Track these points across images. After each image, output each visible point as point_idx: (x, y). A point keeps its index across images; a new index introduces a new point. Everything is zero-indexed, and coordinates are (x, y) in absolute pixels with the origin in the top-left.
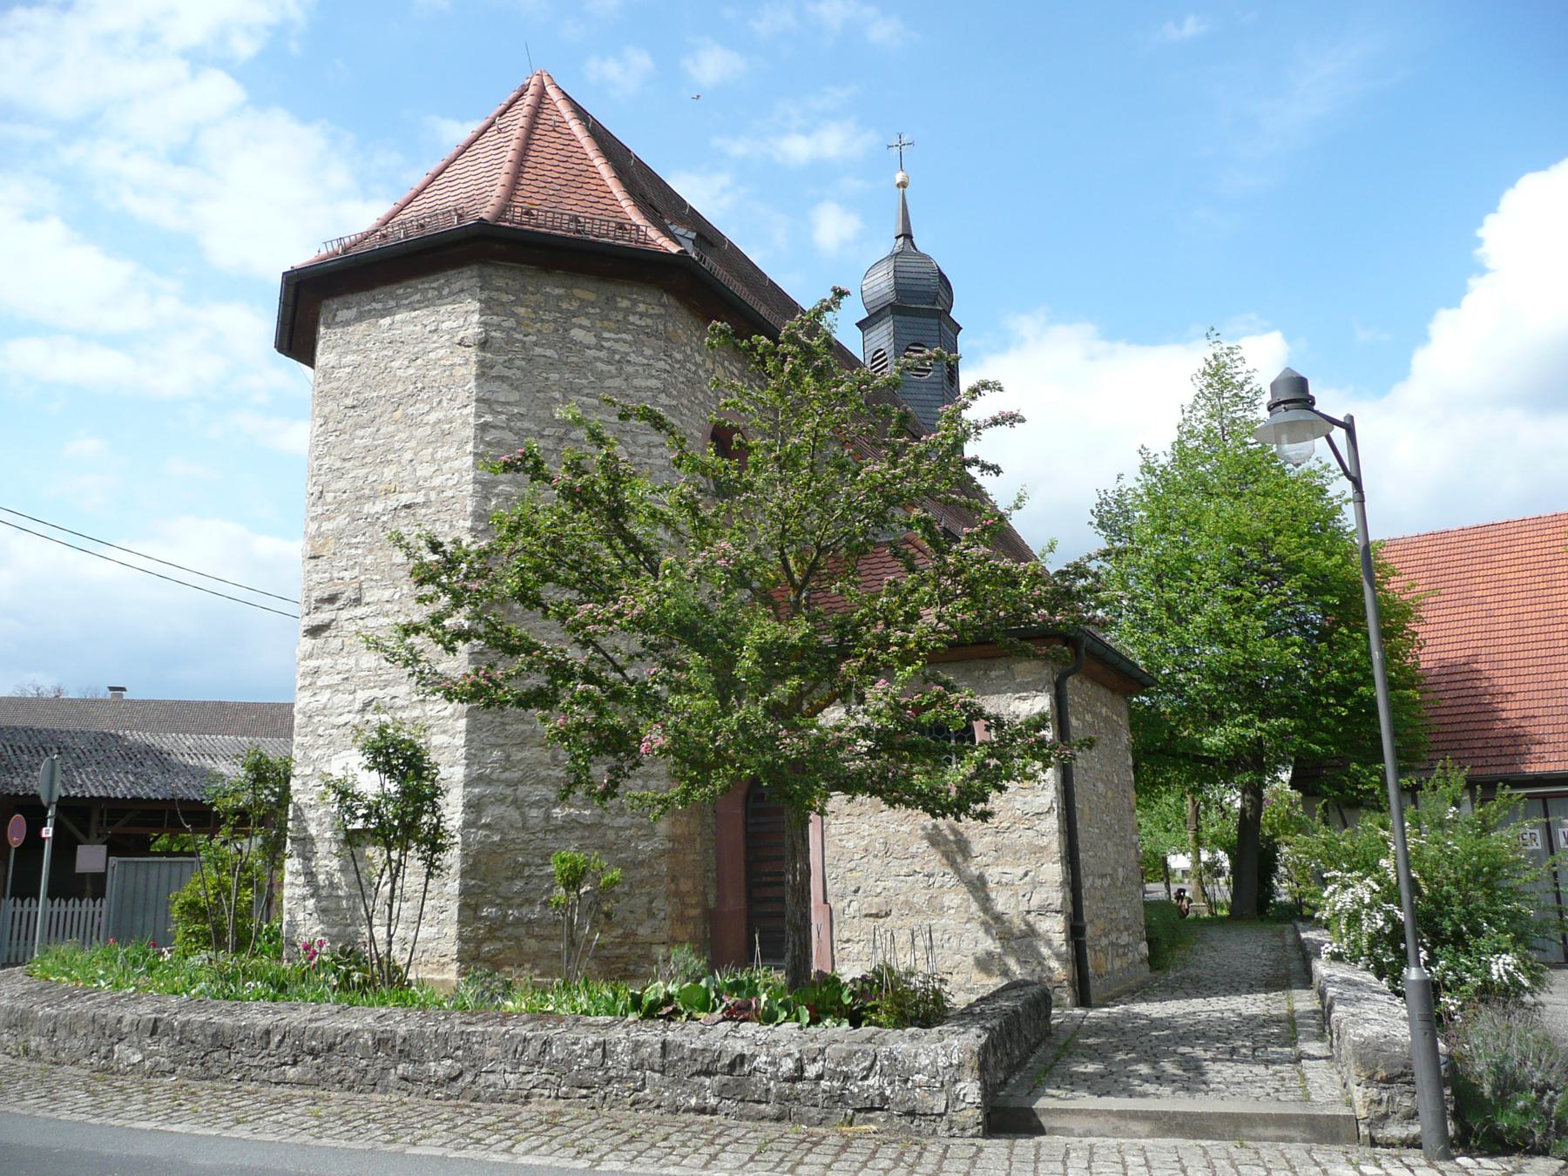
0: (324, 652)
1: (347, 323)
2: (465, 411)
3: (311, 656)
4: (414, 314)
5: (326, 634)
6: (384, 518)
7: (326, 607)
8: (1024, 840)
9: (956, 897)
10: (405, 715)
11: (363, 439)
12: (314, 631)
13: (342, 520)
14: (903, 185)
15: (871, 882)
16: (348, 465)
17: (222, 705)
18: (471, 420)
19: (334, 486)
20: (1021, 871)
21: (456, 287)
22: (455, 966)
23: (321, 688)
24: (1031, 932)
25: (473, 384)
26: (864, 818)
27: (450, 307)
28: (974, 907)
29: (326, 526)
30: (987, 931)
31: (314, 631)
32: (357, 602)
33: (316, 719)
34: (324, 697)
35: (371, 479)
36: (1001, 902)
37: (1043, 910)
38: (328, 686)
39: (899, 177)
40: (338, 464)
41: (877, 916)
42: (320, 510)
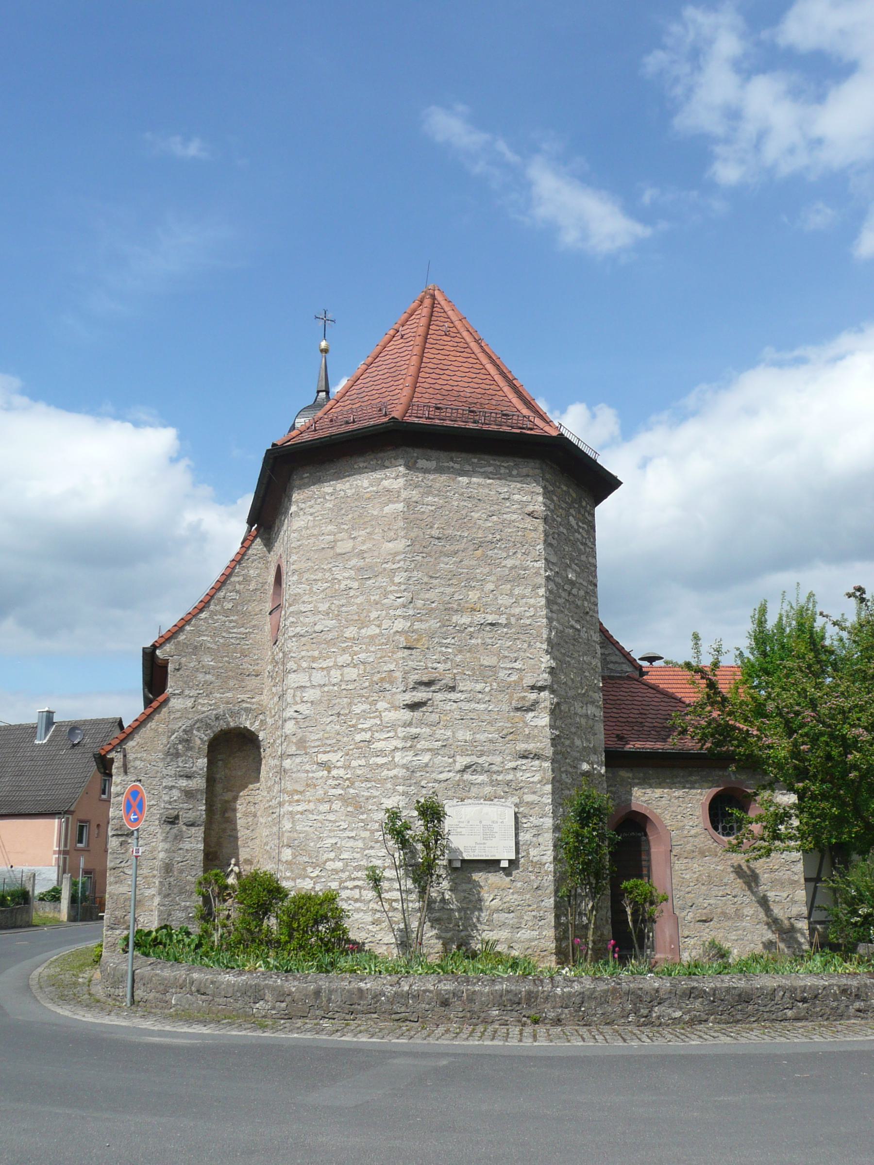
0: (421, 723)
1: (426, 471)
2: (537, 565)
3: (410, 724)
5: (424, 709)
6: (472, 629)
7: (423, 688)
8: (786, 877)
9: (752, 910)
10: (500, 778)
11: (446, 565)
12: (414, 706)
13: (434, 624)
14: (325, 351)
15: (701, 900)
16: (435, 582)
18: (542, 572)
19: (422, 596)
20: (786, 895)
21: (524, 471)
22: (554, 958)
24: (792, 929)
25: (541, 546)
26: (695, 860)
27: (519, 485)
28: (762, 915)
29: (417, 625)
31: (414, 706)
32: (453, 689)
33: (418, 774)
34: (426, 758)
35: (456, 597)
36: (777, 911)
37: (798, 917)
39: (323, 344)
40: (426, 579)
41: (705, 921)
42: (411, 612)
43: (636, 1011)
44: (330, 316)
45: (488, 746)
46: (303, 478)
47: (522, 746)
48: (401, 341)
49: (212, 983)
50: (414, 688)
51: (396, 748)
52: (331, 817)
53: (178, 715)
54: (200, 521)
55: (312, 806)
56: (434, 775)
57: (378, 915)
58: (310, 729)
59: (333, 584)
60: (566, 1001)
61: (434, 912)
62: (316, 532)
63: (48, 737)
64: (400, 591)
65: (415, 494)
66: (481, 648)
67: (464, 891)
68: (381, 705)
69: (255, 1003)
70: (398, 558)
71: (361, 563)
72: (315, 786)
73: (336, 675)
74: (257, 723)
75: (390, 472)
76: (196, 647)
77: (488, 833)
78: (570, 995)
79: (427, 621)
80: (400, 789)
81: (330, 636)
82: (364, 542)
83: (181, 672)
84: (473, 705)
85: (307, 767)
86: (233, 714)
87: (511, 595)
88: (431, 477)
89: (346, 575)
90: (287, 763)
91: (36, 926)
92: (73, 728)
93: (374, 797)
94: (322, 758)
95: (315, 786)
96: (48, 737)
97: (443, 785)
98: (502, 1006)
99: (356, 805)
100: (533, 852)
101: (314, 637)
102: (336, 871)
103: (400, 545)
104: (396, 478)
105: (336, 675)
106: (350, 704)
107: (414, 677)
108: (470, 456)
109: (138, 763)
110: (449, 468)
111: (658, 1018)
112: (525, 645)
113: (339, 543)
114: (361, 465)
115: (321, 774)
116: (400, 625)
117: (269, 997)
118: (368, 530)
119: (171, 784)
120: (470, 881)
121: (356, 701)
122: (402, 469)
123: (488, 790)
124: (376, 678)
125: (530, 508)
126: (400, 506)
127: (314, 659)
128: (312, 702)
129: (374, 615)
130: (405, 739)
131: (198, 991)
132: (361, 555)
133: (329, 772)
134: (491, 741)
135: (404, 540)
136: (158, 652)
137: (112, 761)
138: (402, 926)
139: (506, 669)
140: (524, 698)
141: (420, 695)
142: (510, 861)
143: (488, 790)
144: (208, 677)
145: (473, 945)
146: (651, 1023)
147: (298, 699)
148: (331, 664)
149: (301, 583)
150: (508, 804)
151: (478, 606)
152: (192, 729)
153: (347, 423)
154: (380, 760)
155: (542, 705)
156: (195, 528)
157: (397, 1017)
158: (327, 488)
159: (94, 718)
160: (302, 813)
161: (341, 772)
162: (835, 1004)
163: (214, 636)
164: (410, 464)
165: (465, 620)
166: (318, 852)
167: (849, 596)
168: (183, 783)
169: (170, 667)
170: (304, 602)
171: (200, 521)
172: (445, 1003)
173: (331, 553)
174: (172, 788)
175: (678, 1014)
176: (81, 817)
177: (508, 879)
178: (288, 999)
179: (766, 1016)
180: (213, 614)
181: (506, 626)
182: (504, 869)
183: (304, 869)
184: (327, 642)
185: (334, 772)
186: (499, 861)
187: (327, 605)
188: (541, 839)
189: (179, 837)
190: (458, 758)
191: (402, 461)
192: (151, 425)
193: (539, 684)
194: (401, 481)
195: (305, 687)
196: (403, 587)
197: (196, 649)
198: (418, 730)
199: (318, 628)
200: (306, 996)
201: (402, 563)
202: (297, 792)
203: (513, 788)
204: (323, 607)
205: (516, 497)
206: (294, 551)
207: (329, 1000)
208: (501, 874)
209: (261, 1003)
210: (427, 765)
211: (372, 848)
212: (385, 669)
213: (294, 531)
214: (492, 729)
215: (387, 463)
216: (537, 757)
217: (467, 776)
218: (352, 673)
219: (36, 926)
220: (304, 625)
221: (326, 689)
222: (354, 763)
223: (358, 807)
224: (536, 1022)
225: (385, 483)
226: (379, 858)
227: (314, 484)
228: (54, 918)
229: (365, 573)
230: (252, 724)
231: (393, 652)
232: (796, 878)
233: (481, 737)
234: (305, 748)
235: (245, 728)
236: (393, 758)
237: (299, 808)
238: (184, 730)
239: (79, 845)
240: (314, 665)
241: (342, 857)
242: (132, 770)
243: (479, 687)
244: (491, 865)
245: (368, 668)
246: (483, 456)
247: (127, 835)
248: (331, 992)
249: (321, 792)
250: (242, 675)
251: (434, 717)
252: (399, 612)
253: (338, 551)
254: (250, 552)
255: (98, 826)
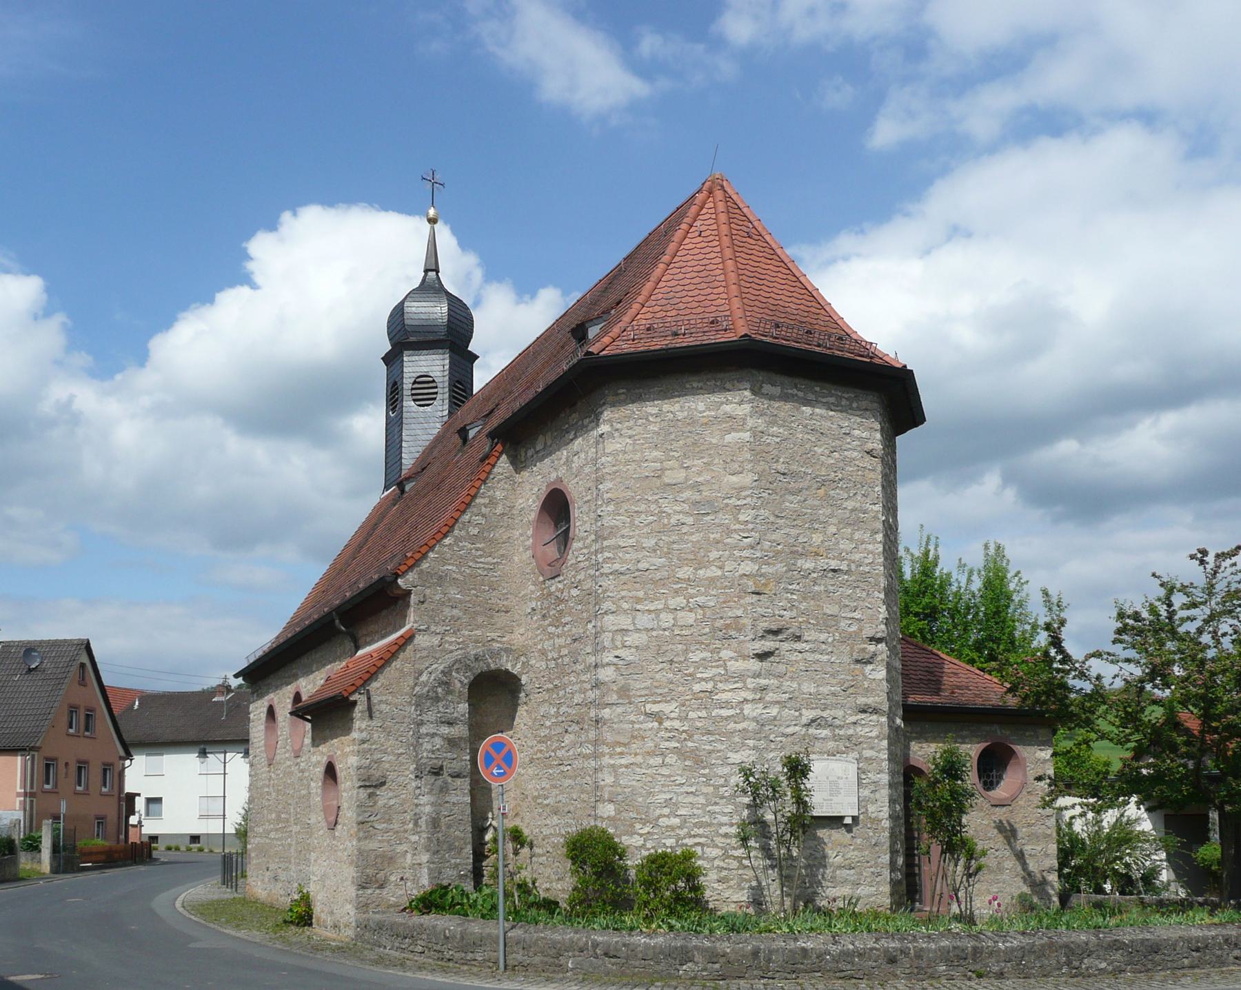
0: (770, 674)
1: (771, 398)
4: (831, 413)
5: (772, 659)
6: (815, 575)
7: (770, 637)
9: (1011, 863)
10: (841, 733)
11: (791, 503)
12: (763, 656)
13: (780, 568)
16: (781, 521)
17: (56, 641)
21: (864, 404)
23: (771, 703)
24: (1044, 882)
25: (879, 488)
27: (859, 420)
28: (1019, 868)
29: (765, 569)
30: (1025, 882)
32: (798, 638)
33: (767, 728)
34: (774, 711)
36: (1032, 866)
37: (1050, 870)
38: (778, 702)
39: (432, 212)
40: (772, 519)
42: (759, 555)
43: (1069, 963)
44: (438, 177)
45: (831, 700)
46: (617, 395)
47: (862, 700)
48: (700, 239)
49: (624, 945)
50: (763, 636)
51: (746, 700)
52: (665, 771)
53: (425, 653)
55: (639, 759)
56: (782, 729)
57: (724, 873)
58: (635, 677)
60: (1009, 955)
61: (783, 867)
64: (748, 531)
65: (760, 423)
69: (682, 965)
70: (743, 494)
71: (697, 497)
72: (643, 738)
74: (519, 666)
76: (441, 577)
77: (834, 789)
78: (1013, 949)
79: (774, 565)
80: (751, 743)
81: (658, 576)
82: (699, 474)
83: (425, 605)
84: (818, 656)
85: (632, 718)
86: (495, 654)
87: (851, 540)
88: (777, 405)
89: (678, 508)
91: (23, 879)
93: (719, 751)
94: (651, 708)
95: (643, 738)
97: (789, 739)
98: (949, 962)
99: (697, 760)
100: (871, 808)
101: (637, 577)
102: (672, 828)
103: (747, 479)
105: (667, 619)
106: (686, 651)
107: (763, 625)
108: (813, 383)
110: (793, 396)
111: (1087, 969)
113: (667, 473)
114: (695, 385)
115: (650, 725)
116: (748, 567)
117: (698, 957)
118: (705, 460)
119: (432, 731)
122: (747, 393)
123: (831, 745)
125: (869, 446)
126: (746, 436)
127: (638, 600)
128: (637, 647)
129: (714, 555)
130: (754, 690)
131: (606, 954)
132: (696, 486)
133: (660, 723)
134: (834, 694)
135: (751, 475)
136: (400, 581)
137: (355, 703)
138: (754, 883)
140: (864, 650)
142: (854, 818)
143: (831, 745)
144: (455, 612)
145: (818, 902)
147: (619, 644)
148: (661, 607)
149: (619, 514)
150: (849, 759)
151: (821, 550)
152: (450, 671)
154: (725, 713)
155: (879, 658)
156: (66, 407)
157: (842, 974)
158: (651, 408)
159: (68, 637)
160: (626, 767)
161: (677, 724)
162: (1219, 953)
164: (756, 389)
165: (808, 564)
166: (648, 808)
167: (1192, 557)
168: (445, 730)
169: (413, 599)
170: (623, 537)
172: (892, 961)
173: (658, 482)
174: (433, 735)
175: (1103, 965)
176: (48, 755)
178: (722, 960)
180: (458, 540)
181: (846, 573)
182: (846, 825)
183: (632, 826)
184: (654, 582)
185: (667, 724)
186: (842, 818)
187: (653, 542)
188: (878, 795)
189: (444, 789)
191: (748, 385)
193: (879, 635)
194: (747, 408)
195: (627, 630)
196: (750, 526)
197: (441, 579)
199: (642, 566)
200: (743, 956)
201: (749, 499)
202: (619, 744)
203: (852, 743)
204: (650, 543)
205: (856, 432)
206: (608, 477)
207: (769, 960)
208: (843, 830)
209: (690, 964)
210: (775, 718)
211: (716, 804)
212: (730, 614)
214: (834, 681)
215: (728, 385)
216: (876, 711)
217: (812, 731)
218: (690, 618)
219: (23, 879)
220: (623, 562)
221: (654, 633)
222: (692, 715)
223: (699, 762)
224: (980, 976)
226: (725, 814)
227: (633, 402)
229: (703, 508)
230: (514, 666)
231: (740, 597)
232: (1049, 832)
233: (825, 690)
234: (629, 697)
235: (507, 672)
236: (742, 710)
237: (623, 761)
238: (442, 672)
239: (46, 786)
240: (638, 607)
241: (679, 813)
242: (377, 714)
243: (823, 637)
244: (835, 821)
245: (708, 613)
247: (375, 786)
249: (651, 744)
250: (492, 611)
251: (782, 668)
252: (745, 553)
253: (667, 480)
255: (67, 764)
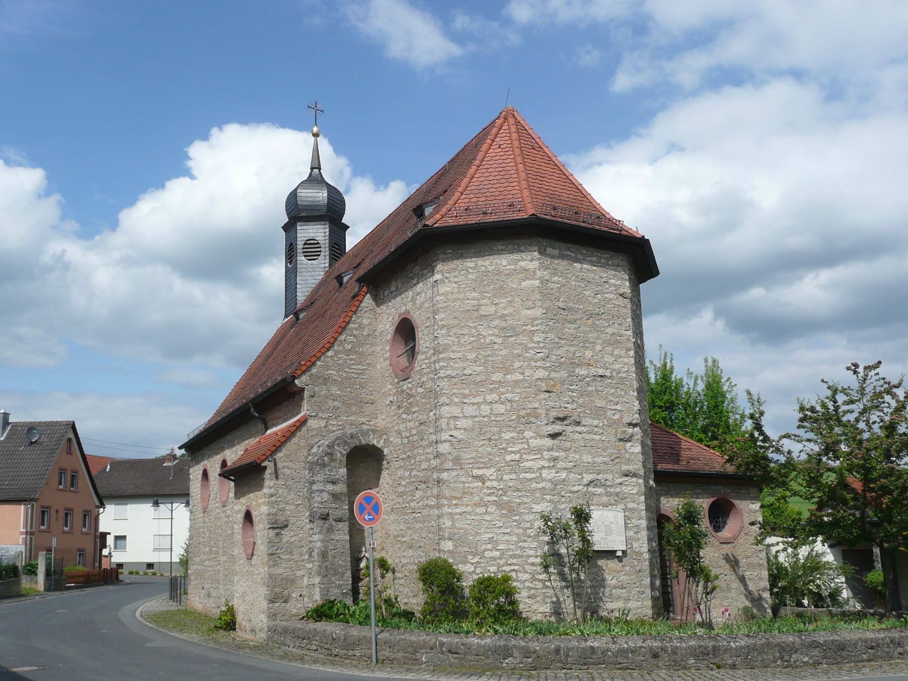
0: (559, 449)
3: (552, 449)
4: (595, 268)
5: (560, 438)
7: (559, 422)
10: (612, 490)
11: (570, 329)
12: (554, 436)
13: (564, 374)
16: (561, 341)
21: (617, 262)
24: (760, 598)
25: (629, 320)
27: (614, 273)
28: (742, 588)
29: (553, 375)
32: (578, 423)
33: (559, 487)
34: (563, 475)
36: (751, 587)
39: (315, 129)
40: (556, 340)
42: (548, 365)
43: (781, 658)
47: (625, 468)
48: (499, 150)
49: (463, 644)
51: (543, 467)
52: (487, 518)
53: (315, 432)
54: (64, 252)
55: (469, 509)
56: (569, 488)
57: (533, 591)
59: (479, 339)
62: (461, 296)
63: (5, 435)
64: (540, 348)
65: (546, 274)
66: (595, 394)
67: (593, 573)
68: (528, 434)
70: (536, 322)
71: (504, 324)
72: (472, 494)
73: (485, 410)
74: (382, 442)
75: (527, 256)
76: (325, 379)
77: (609, 531)
78: (741, 648)
80: (548, 497)
82: (505, 308)
83: (315, 398)
84: (593, 436)
85: (463, 479)
86: (365, 434)
87: (612, 355)
88: (556, 262)
90: (445, 475)
92: (31, 428)
93: (525, 503)
94: (479, 472)
95: (472, 494)
96: (5, 435)
97: (575, 495)
98: (696, 657)
99: (510, 510)
100: (635, 545)
101: (463, 379)
102: (494, 559)
103: (538, 312)
104: (531, 260)
105: (485, 410)
106: (500, 432)
107: (554, 414)
109: (286, 470)
110: (568, 256)
111: (795, 662)
112: (623, 393)
113: (482, 308)
114: (500, 248)
115: (476, 485)
116: (541, 374)
117: (516, 654)
119: (321, 488)
120: (597, 566)
121: (505, 430)
123: (605, 499)
124: (522, 413)
125: (622, 291)
126: (537, 283)
127: (465, 396)
128: (465, 429)
129: (517, 364)
130: (549, 460)
131: (449, 651)
132: (503, 317)
133: (483, 483)
134: (605, 463)
137: (265, 468)
138: (554, 599)
139: (611, 409)
140: (625, 432)
141: (557, 428)
142: (623, 551)
143: (605, 499)
144: (336, 403)
146: (791, 666)
147: (452, 426)
149: (450, 336)
151: (592, 362)
153: (485, 213)
155: (636, 438)
157: (620, 666)
158: (470, 263)
160: (460, 514)
161: (495, 484)
162: (887, 650)
163: (339, 371)
165: (583, 372)
167: (848, 369)
168: (330, 487)
170: (453, 351)
171: (64, 252)
172: (656, 656)
173: (476, 314)
174: (322, 491)
175: (806, 659)
176: (43, 504)
177: (620, 564)
178: (534, 656)
179: (853, 659)
180: (337, 353)
181: (610, 378)
182: (618, 557)
183: (465, 557)
184: (476, 383)
185: (488, 484)
187: (474, 355)
188: (639, 536)
189: (330, 530)
190: (584, 475)
191: (536, 248)
192: (20, 165)
193: (634, 422)
194: (536, 264)
196: (542, 345)
198: (557, 454)
199: (466, 372)
200: (548, 652)
203: (620, 498)
207: (567, 656)
208: (616, 561)
209: (510, 659)
210: (564, 480)
211: (525, 541)
213: (441, 295)
214: (605, 454)
216: (635, 475)
217: (591, 489)
218: (502, 409)
220: (454, 369)
221: (477, 419)
222: (506, 477)
223: (512, 511)
225: (523, 264)
226: (531, 549)
227: (457, 259)
228: (31, 589)
229: (508, 332)
230: (378, 442)
231: (536, 394)
232: (761, 562)
233: (599, 460)
234: (460, 464)
235: (373, 446)
236: (541, 474)
237: (458, 510)
239: (42, 527)
240: (465, 401)
241: (499, 548)
242: (281, 476)
243: (595, 422)
245: (515, 405)
246: (591, 249)
247: (281, 528)
248: (568, 649)
250: (362, 403)
251: (568, 444)
252: (538, 364)
253: (482, 313)
254: (362, 305)
255: (57, 511)
